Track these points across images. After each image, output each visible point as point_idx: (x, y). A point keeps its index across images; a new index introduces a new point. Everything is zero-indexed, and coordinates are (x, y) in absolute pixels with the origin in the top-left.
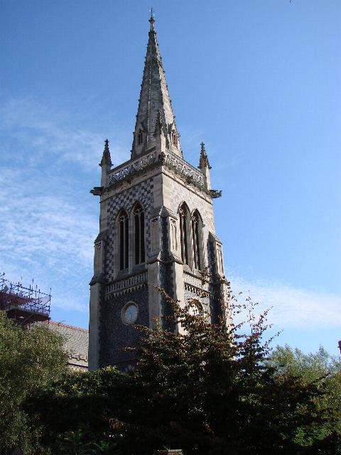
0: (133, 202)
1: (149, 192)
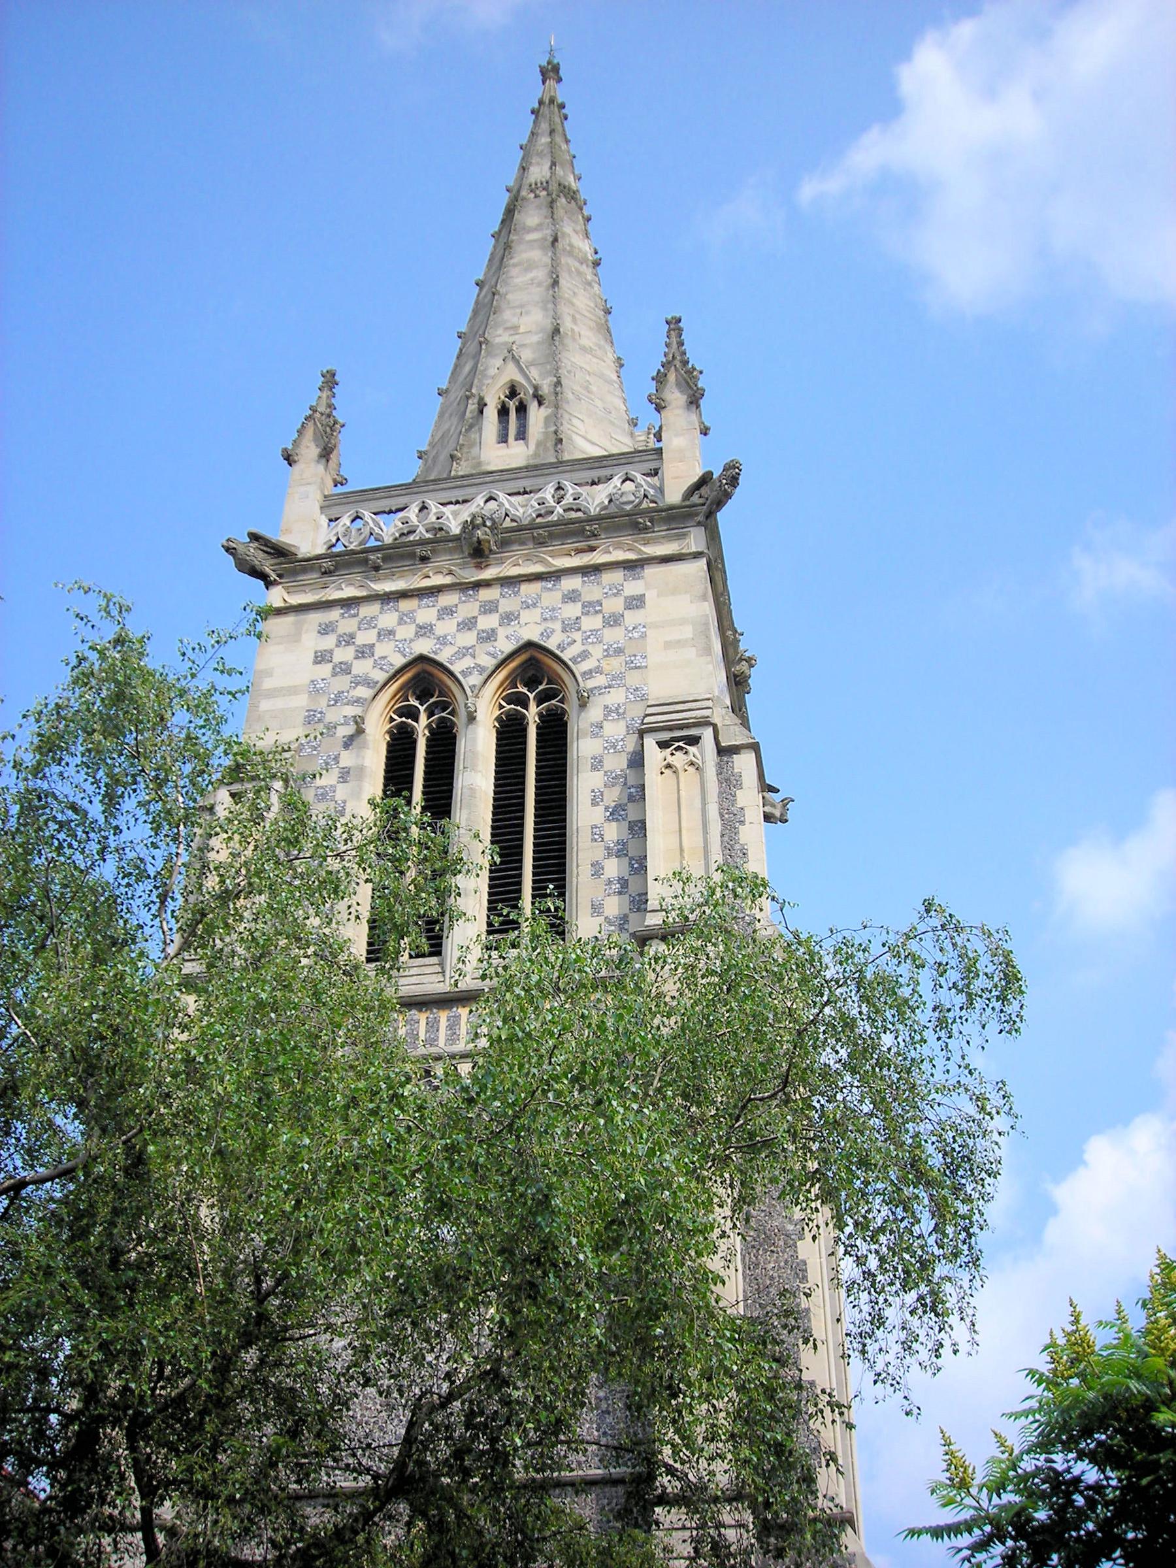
0: (506, 646)
1: (614, 621)
